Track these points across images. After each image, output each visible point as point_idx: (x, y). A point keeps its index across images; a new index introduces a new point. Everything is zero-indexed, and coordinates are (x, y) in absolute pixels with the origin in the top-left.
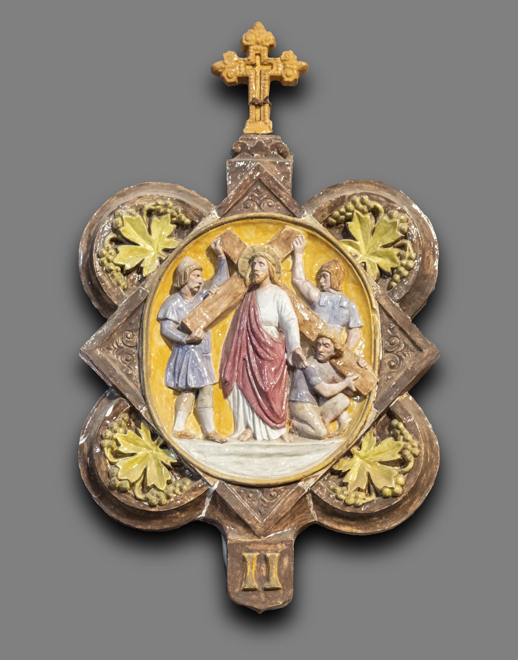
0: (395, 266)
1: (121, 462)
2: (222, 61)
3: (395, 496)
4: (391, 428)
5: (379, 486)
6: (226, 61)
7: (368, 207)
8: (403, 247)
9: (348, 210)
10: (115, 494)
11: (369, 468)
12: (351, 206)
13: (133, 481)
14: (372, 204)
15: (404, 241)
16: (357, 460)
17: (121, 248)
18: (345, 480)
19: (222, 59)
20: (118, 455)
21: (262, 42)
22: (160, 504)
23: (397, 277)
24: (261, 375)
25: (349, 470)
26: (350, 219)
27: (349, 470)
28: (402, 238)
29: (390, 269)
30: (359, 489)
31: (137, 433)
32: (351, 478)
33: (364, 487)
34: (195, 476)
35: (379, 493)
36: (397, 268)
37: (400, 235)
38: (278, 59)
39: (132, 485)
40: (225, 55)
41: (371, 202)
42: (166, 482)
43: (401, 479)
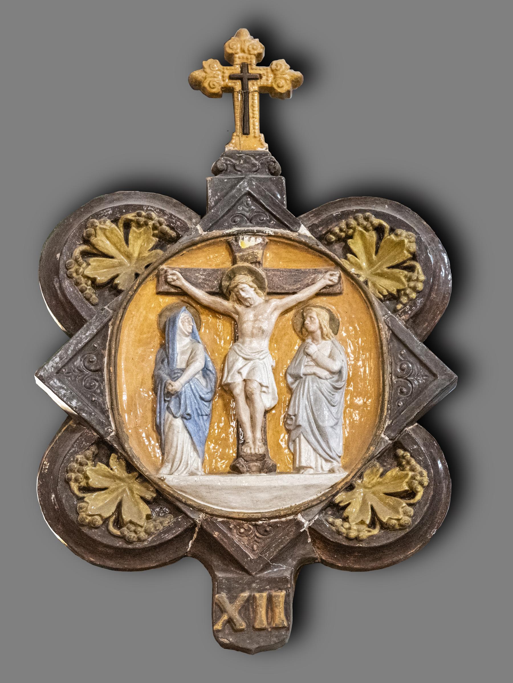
0: (401, 287)
1: (89, 497)
2: (202, 70)
3: (403, 527)
4: (396, 457)
5: (385, 519)
6: (208, 70)
7: (372, 225)
8: (411, 269)
9: (348, 225)
10: (85, 530)
11: (373, 501)
12: (353, 222)
13: (106, 515)
14: (376, 221)
15: (413, 263)
16: (359, 493)
17: (91, 260)
18: (345, 514)
19: (202, 67)
20: (88, 489)
21: (249, 51)
22: (139, 540)
23: (404, 300)
24: (329, 448)
25: (349, 504)
26: (351, 237)
27: (349, 504)
28: (410, 259)
29: (395, 290)
30: (362, 522)
31: (108, 465)
32: (353, 511)
33: (368, 522)
34: (176, 510)
35: (384, 526)
36: (404, 290)
37: (410, 256)
38: (269, 68)
39: (106, 521)
40: (205, 64)
41: (375, 219)
42: (144, 517)
43: (411, 511)
